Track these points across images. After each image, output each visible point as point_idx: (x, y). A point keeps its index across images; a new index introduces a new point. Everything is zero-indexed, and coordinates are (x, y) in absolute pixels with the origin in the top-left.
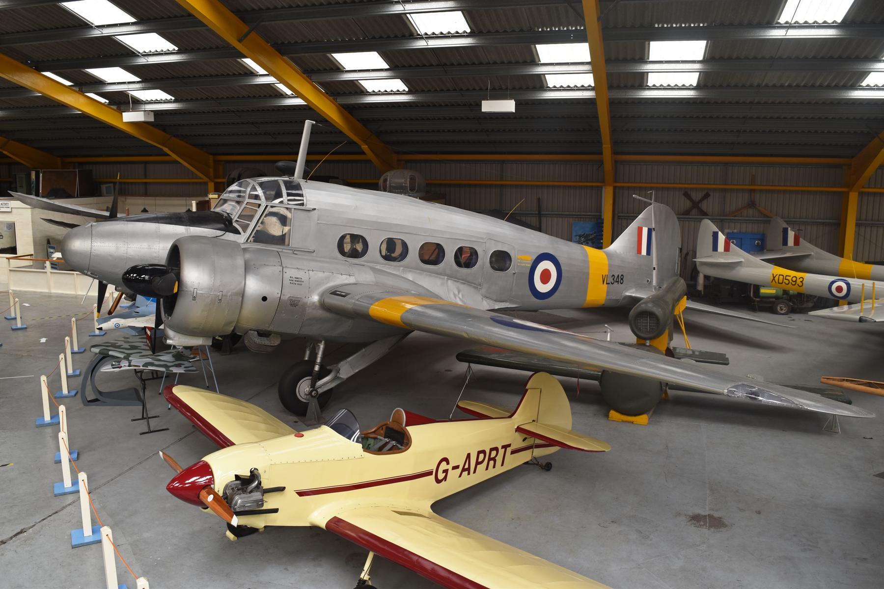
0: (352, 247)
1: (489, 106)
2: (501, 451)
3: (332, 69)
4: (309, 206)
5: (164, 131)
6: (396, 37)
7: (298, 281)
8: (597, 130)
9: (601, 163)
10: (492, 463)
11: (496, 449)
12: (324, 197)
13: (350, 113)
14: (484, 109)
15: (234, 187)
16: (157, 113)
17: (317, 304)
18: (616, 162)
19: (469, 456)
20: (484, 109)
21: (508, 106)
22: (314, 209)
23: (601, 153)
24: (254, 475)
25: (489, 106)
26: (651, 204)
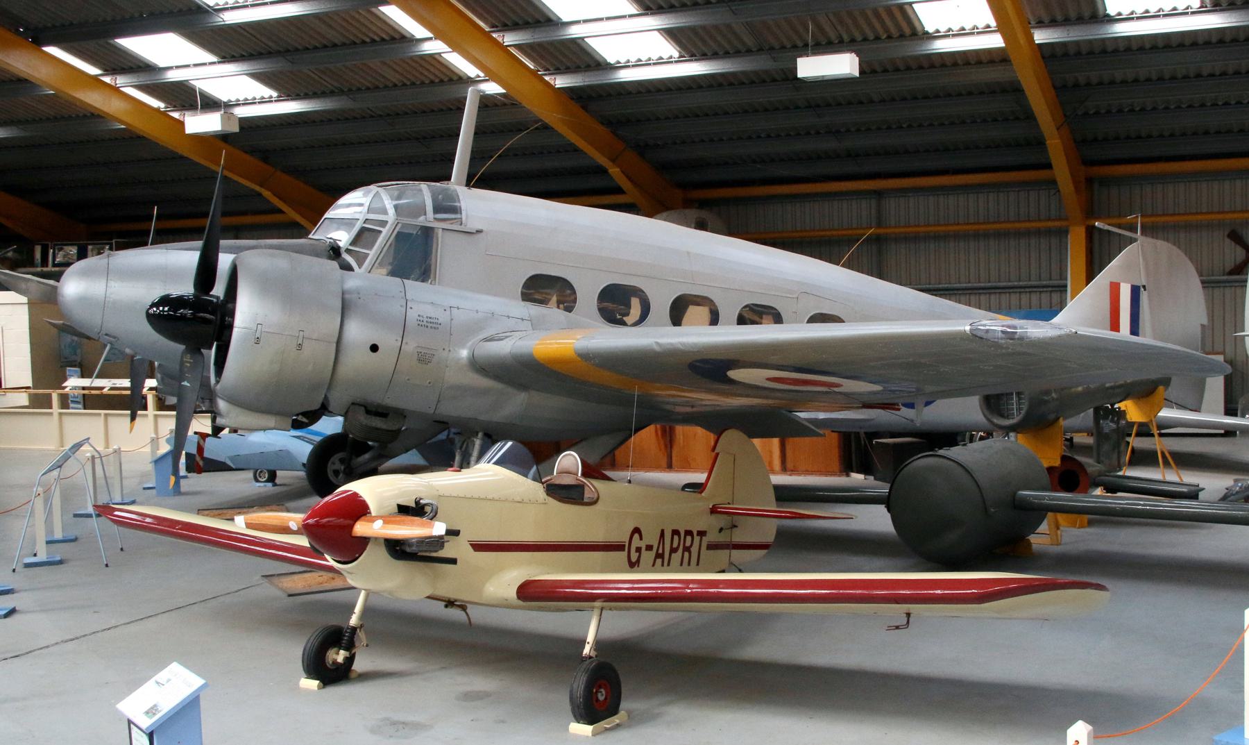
0: (545, 288)
1: (811, 67)
2: (697, 539)
3: (538, 22)
4: (472, 225)
6: (783, 47)
7: (430, 325)
8: (1030, 117)
9: (1053, 183)
10: (686, 554)
11: (688, 533)
12: (487, 208)
13: (584, 108)
14: (801, 73)
15: (354, 205)
17: (465, 361)
20: (801, 73)
21: (843, 65)
22: (479, 232)
23: (1049, 166)
24: (446, 606)
25: (811, 67)
26: (1136, 240)
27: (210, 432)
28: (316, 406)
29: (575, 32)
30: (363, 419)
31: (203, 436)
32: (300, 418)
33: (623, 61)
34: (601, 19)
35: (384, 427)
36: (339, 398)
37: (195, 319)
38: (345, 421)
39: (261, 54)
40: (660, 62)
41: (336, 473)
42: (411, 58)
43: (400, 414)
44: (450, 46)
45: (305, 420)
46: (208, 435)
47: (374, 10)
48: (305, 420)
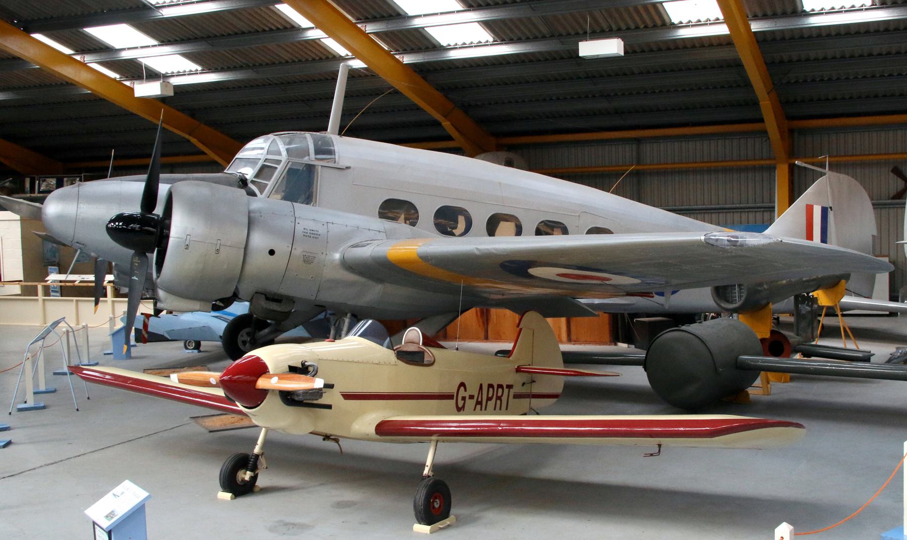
0: (396, 209)
1: (589, 49)
3: (391, 16)
4: (343, 163)
5: (193, 116)
6: (569, 34)
7: (312, 235)
8: (748, 85)
9: (764, 132)
12: (354, 151)
13: (424, 78)
14: (582, 53)
16: (177, 88)
17: (338, 262)
18: (791, 131)
19: (481, 385)
20: (582, 53)
21: (612, 47)
22: (348, 168)
25: (589, 49)
26: (825, 174)
27: (152, 313)
28: (230, 294)
29: (417, 23)
30: (264, 303)
31: (148, 316)
32: (218, 303)
33: (452, 44)
34: (437, 14)
35: (279, 309)
36: (246, 288)
37: (141, 231)
38: (251, 305)
39: (190, 39)
40: (479, 45)
41: (244, 343)
42: (299, 42)
43: (291, 300)
45: (221, 304)
46: (151, 315)
47: (271, 7)
48: (221, 304)
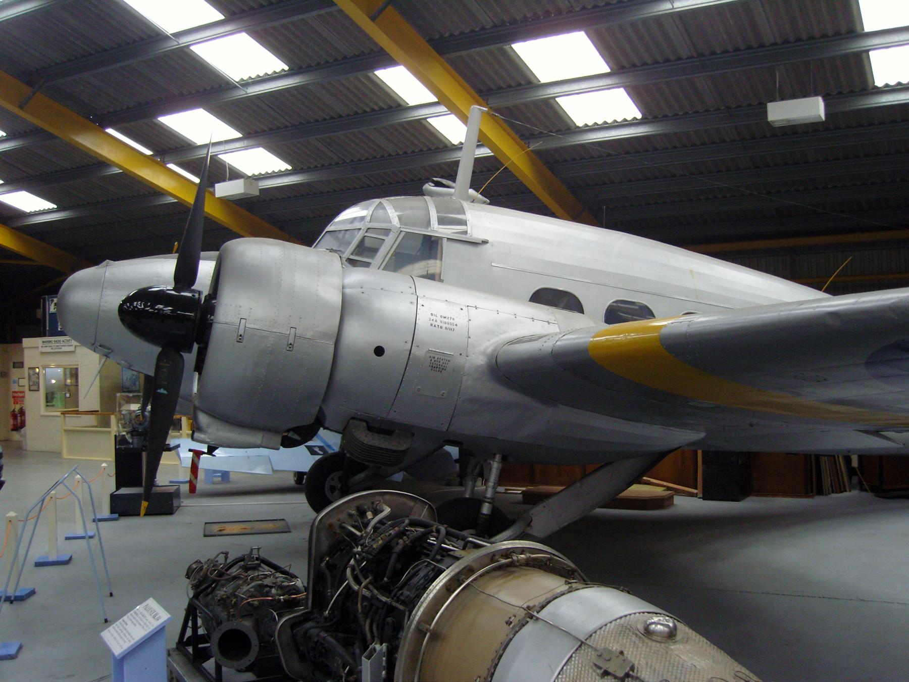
1: (781, 112)
12: (493, 224)
25: (781, 112)
27: (206, 451)
28: (310, 420)
30: (365, 437)
31: (197, 454)
32: (290, 435)
35: (389, 447)
36: (335, 410)
37: (172, 317)
38: (343, 439)
41: (333, 489)
43: (408, 431)
44: (449, 110)
45: (296, 437)
46: (204, 453)
48: (296, 437)
